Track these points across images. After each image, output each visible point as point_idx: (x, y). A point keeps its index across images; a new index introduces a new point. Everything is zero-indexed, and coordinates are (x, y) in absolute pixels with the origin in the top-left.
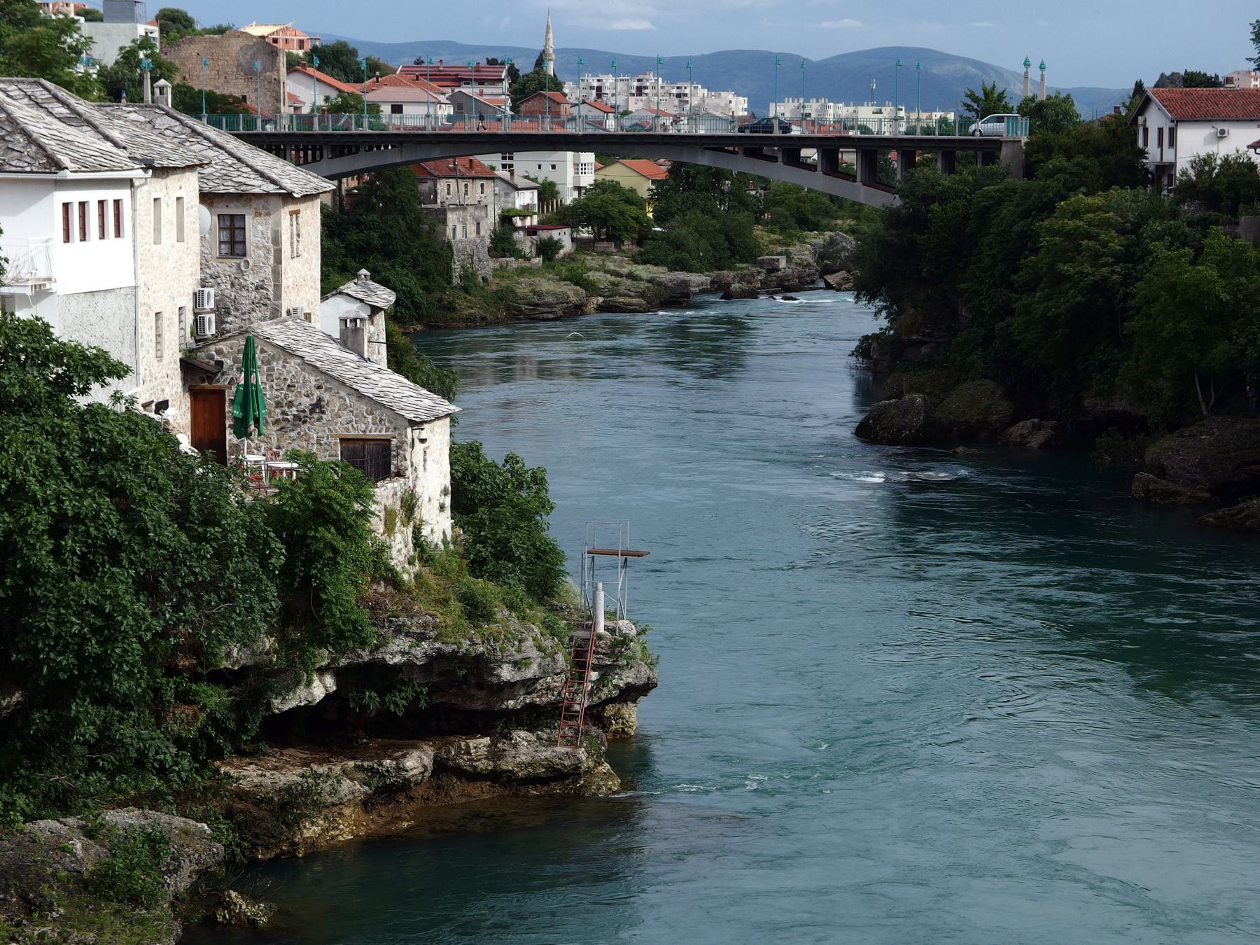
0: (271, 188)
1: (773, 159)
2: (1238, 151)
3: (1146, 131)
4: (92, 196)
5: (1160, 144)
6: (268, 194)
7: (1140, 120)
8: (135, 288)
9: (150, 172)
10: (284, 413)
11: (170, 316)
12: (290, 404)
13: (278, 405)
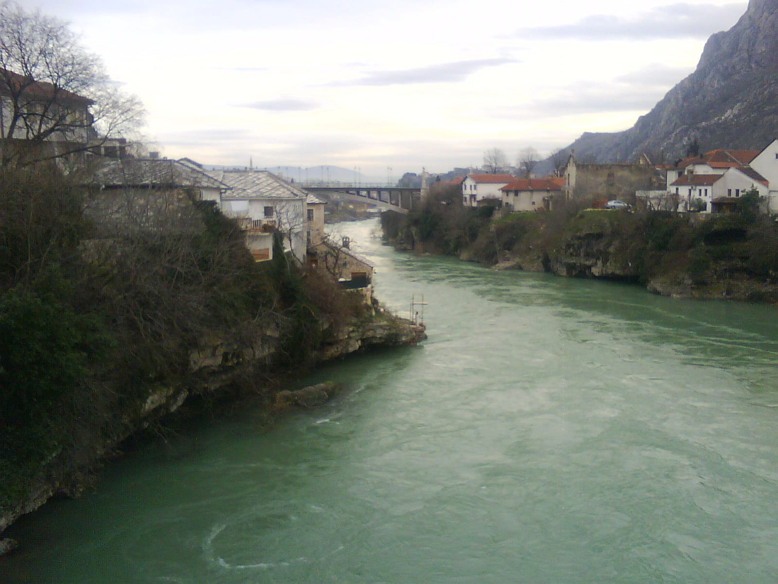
3: (465, 186)
5: (471, 189)
7: (464, 183)
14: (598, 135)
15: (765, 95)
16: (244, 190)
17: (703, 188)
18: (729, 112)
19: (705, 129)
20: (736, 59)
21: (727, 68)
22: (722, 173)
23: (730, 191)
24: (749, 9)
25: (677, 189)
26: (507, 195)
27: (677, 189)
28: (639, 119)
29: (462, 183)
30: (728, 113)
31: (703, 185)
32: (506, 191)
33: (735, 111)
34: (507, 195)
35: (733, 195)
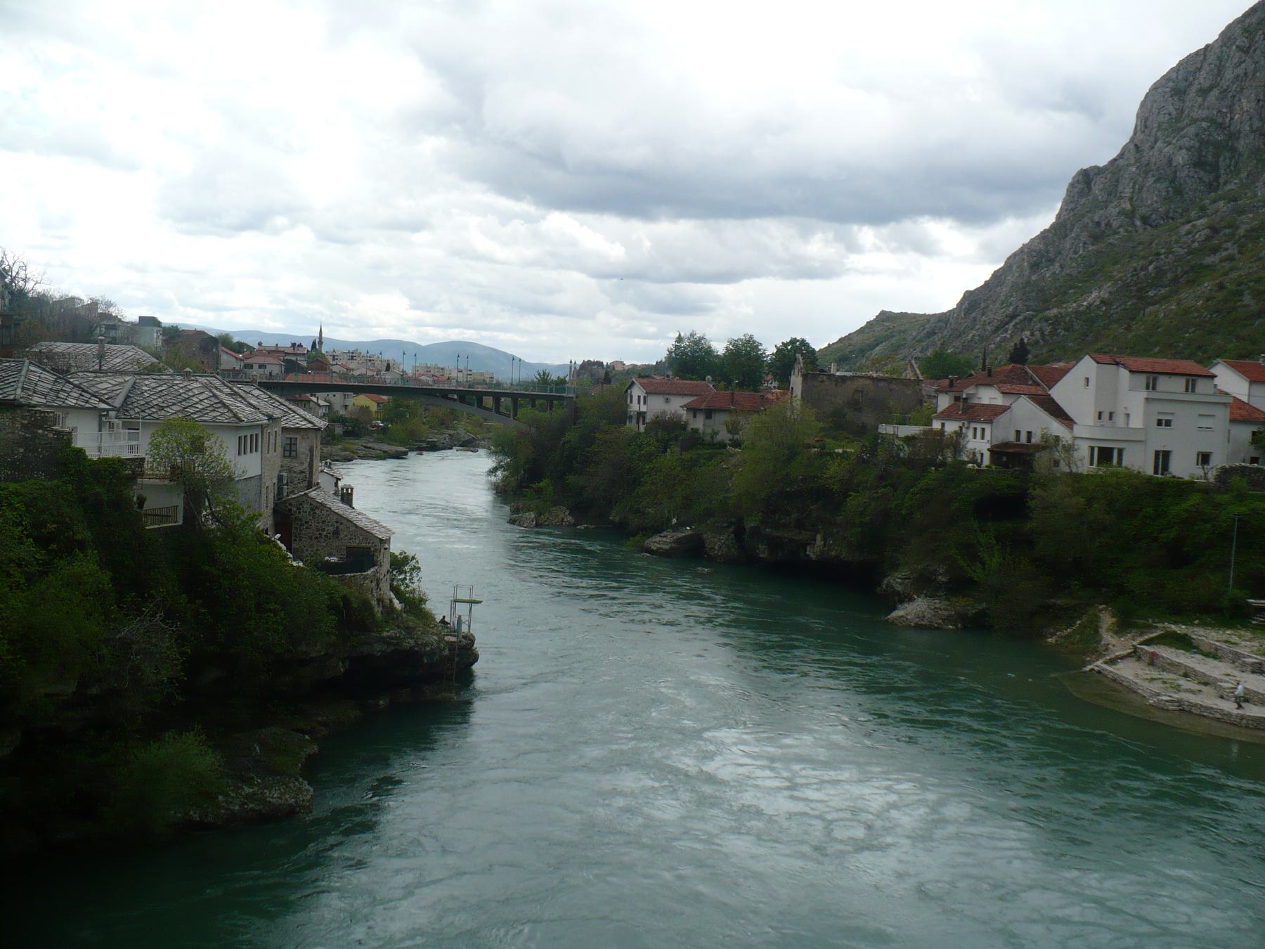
0: (310, 426)
1: (472, 404)
2: (368, 352)
3: (631, 396)
4: (248, 433)
5: (639, 402)
6: (309, 428)
7: (629, 391)
8: (261, 475)
9: (271, 421)
10: (320, 534)
11: (271, 489)
12: (323, 530)
13: (318, 530)
14: (903, 315)
15: (1150, 271)
16: (162, 408)
17: (979, 426)
18: (1095, 294)
19: (1056, 322)
20: (1113, 210)
21: (1098, 224)
22: (1008, 404)
23: (1018, 433)
24: (1135, 133)
25: (943, 425)
26: (695, 417)
27: (943, 425)
28: (964, 295)
29: (626, 391)
30: (1094, 296)
31: (979, 422)
32: (693, 410)
33: (1104, 294)
34: (695, 417)
35: (1023, 440)
